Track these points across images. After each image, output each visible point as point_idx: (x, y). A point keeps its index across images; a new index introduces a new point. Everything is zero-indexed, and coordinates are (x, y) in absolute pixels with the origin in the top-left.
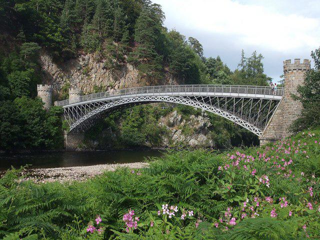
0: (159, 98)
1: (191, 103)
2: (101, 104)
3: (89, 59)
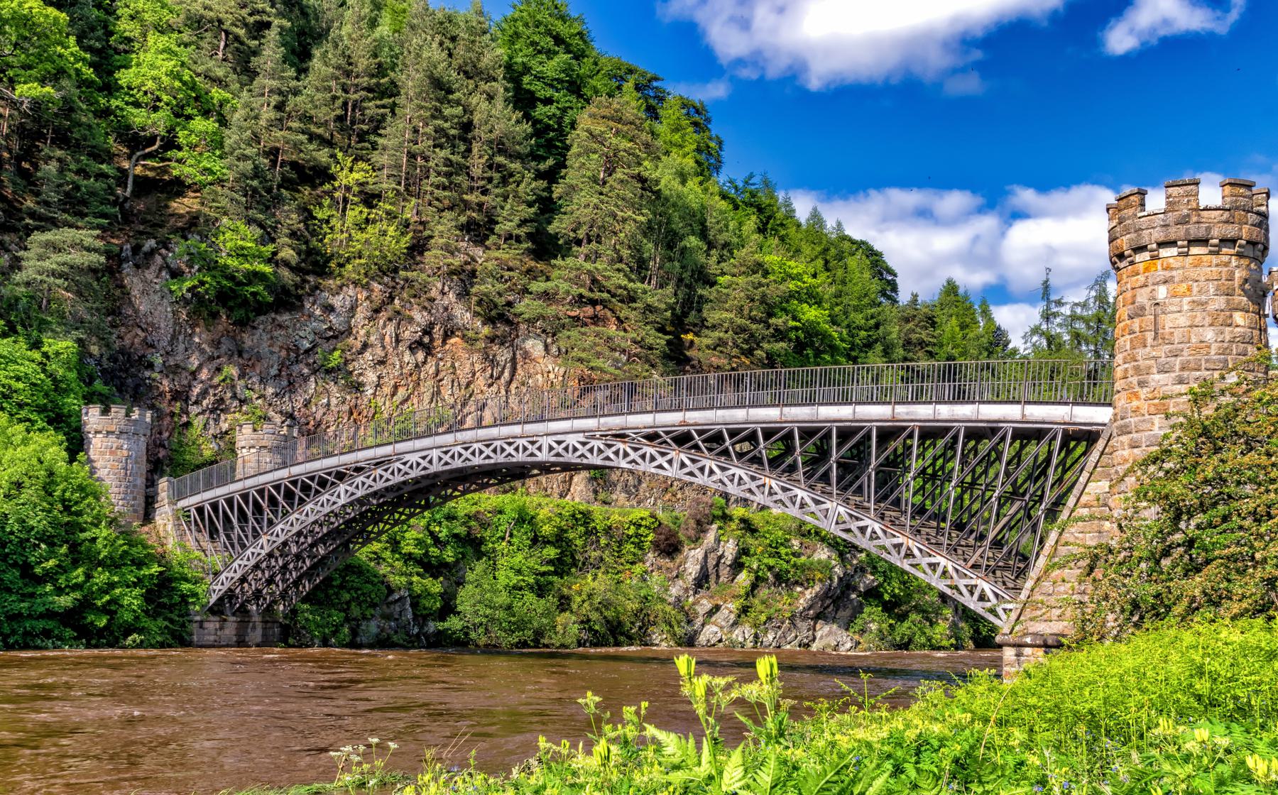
0: (545, 449)
1: (676, 465)
2: (323, 483)
3: (353, 309)
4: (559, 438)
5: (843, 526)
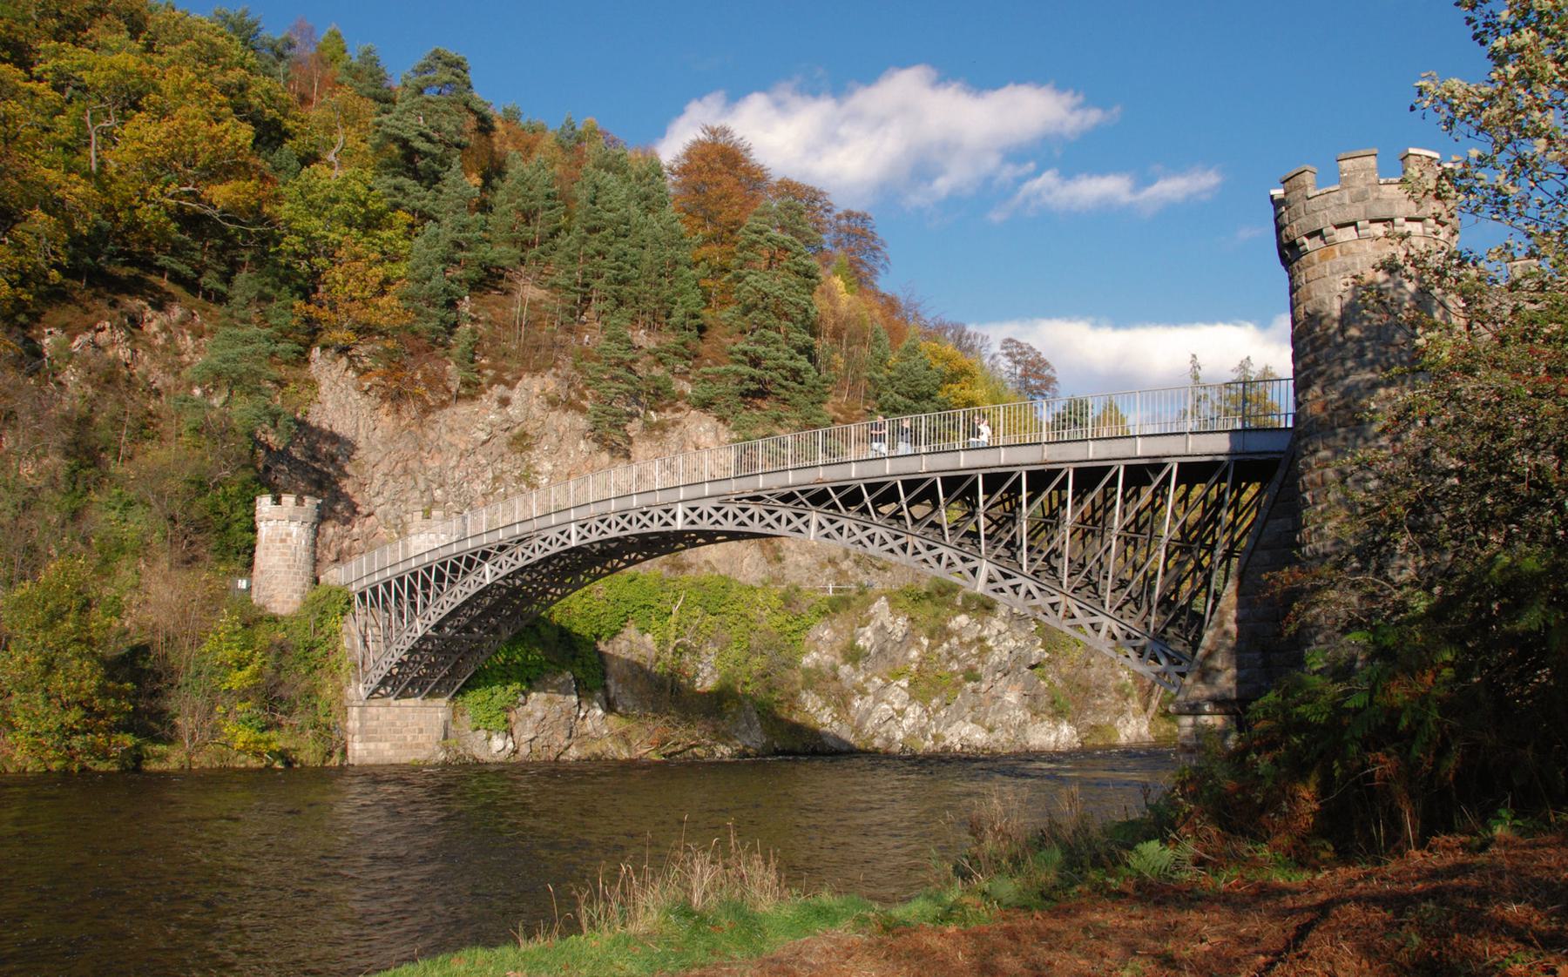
4: (693, 504)
5: (994, 586)
